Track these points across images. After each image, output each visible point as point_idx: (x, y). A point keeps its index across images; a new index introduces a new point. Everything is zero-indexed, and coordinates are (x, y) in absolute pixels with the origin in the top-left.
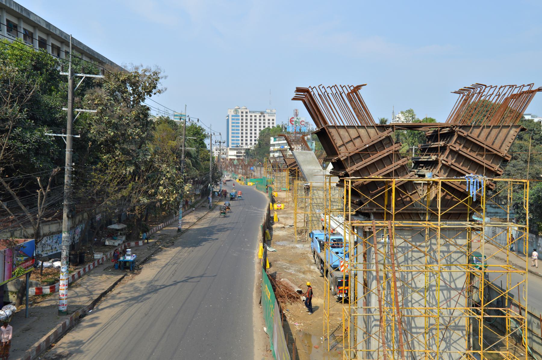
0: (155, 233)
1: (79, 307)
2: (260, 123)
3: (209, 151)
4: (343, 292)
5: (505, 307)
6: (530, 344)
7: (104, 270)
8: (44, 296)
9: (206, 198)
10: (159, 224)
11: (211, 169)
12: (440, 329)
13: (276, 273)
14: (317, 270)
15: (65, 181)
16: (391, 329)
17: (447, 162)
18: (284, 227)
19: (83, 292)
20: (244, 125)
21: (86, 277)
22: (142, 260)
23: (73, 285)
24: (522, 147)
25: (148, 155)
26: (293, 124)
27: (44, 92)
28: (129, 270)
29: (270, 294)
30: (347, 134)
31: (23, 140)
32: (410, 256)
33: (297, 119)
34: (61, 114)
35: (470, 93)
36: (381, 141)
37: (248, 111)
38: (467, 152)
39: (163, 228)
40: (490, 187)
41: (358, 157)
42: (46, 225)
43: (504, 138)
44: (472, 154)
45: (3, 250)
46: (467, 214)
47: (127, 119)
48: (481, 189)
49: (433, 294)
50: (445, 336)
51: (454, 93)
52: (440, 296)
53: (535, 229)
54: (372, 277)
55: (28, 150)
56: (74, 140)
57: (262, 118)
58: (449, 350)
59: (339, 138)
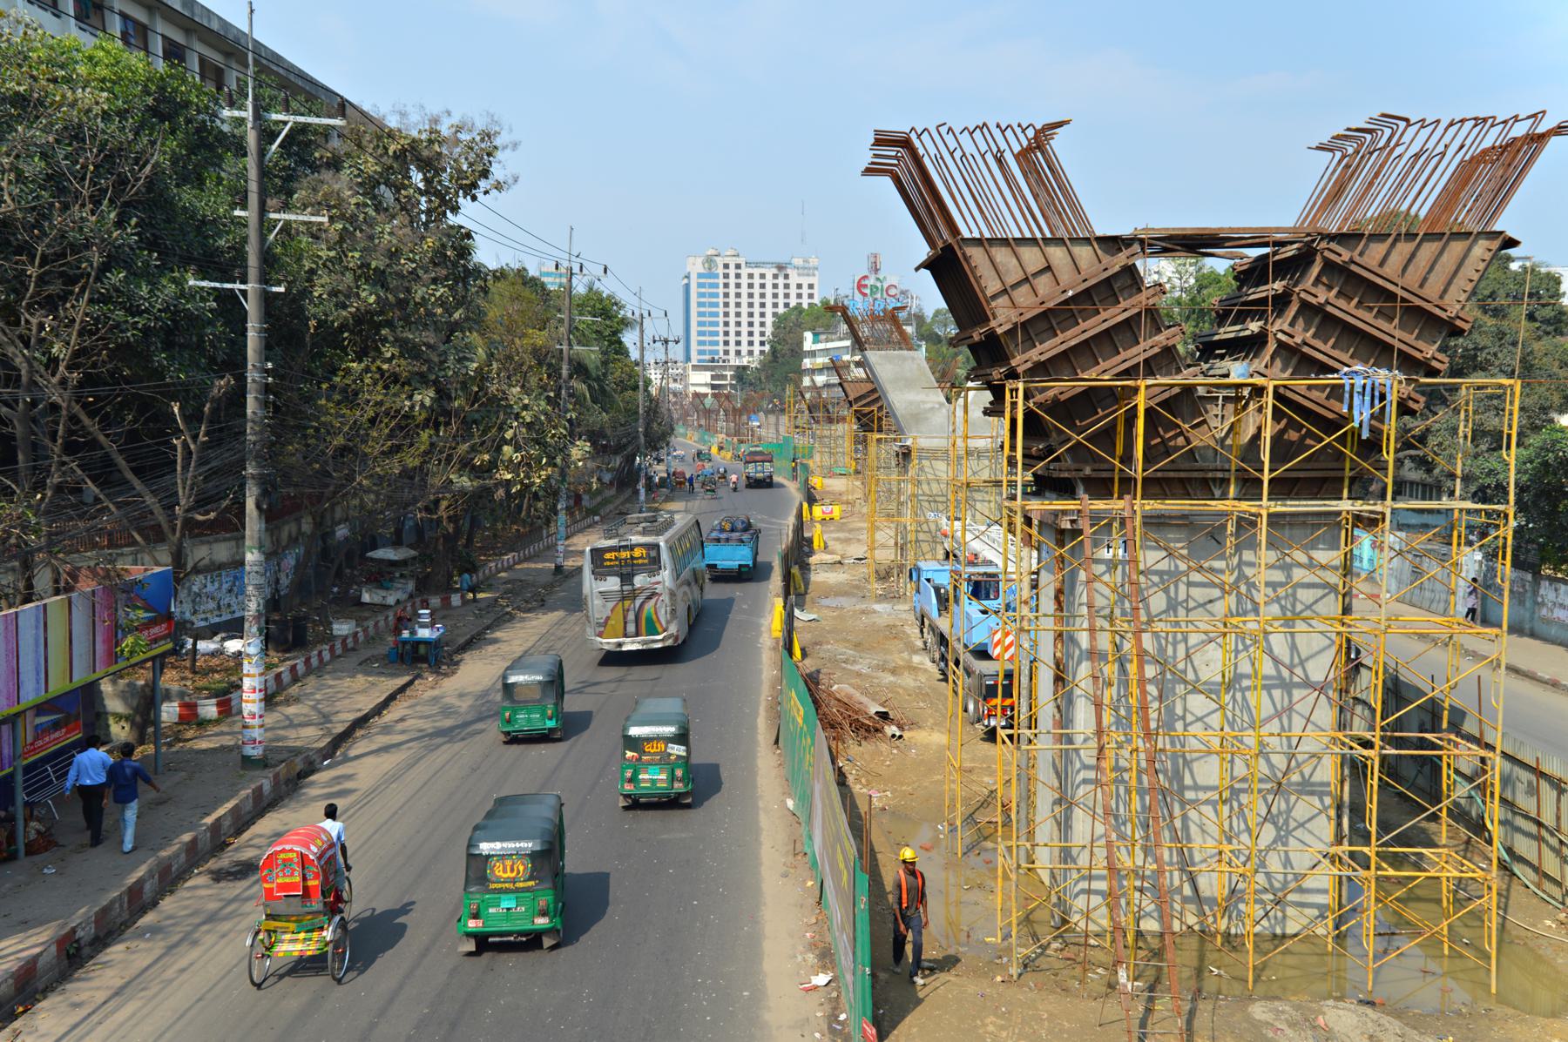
0: (493, 576)
1: (296, 751)
2: (775, 296)
3: (637, 364)
4: (999, 714)
5: (1440, 731)
6: (1506, 840)
7: (360, 664)
8: (203, 724)
9: (629, 491)
10: (506, 554)
11: (641, 411)
12: (1260, 791)
13: (818, 672)
14: (929, 665)
15: (249, 411)
16: (1128, 792)
17: (1293, 337)
18: (840, 563)
19: (305, 715)
20: (732, 300)
21: (312, 681)
22: (462, 640)
23: (278, 699)
24: (1504, 334)
25: (473, 361)
26: (865, 295)
27: (183, 180)
28: (425, 665)
29: (802, 712)
30: (1014, 261)
31: (131, 305)
32: (1182, 596)
33: (878, 279)
34: (231, 237)
35: (1363, 144)
36: (1108, 280)
37: (741, 261)
38: (1349, 310)
39: (515, 564)
40: (1411, 404)
41: (1043, 325)
42: (203, 543)
43: (1454, 268)
44: (1361, 313)
45: (89, 589)
46: (1342, 479)
47: (413, 261)
48: (1384, 406)
49: (1244, 698)
50: (1274, 810)
51: (1318, 148)
52: (1262, 703)
53: (1532, 558)
54: (1077, 652)
55: (146, 331)
56: (268, 300)
57: (781, 281)
58: (1285, 844)
59: (993, 273)
